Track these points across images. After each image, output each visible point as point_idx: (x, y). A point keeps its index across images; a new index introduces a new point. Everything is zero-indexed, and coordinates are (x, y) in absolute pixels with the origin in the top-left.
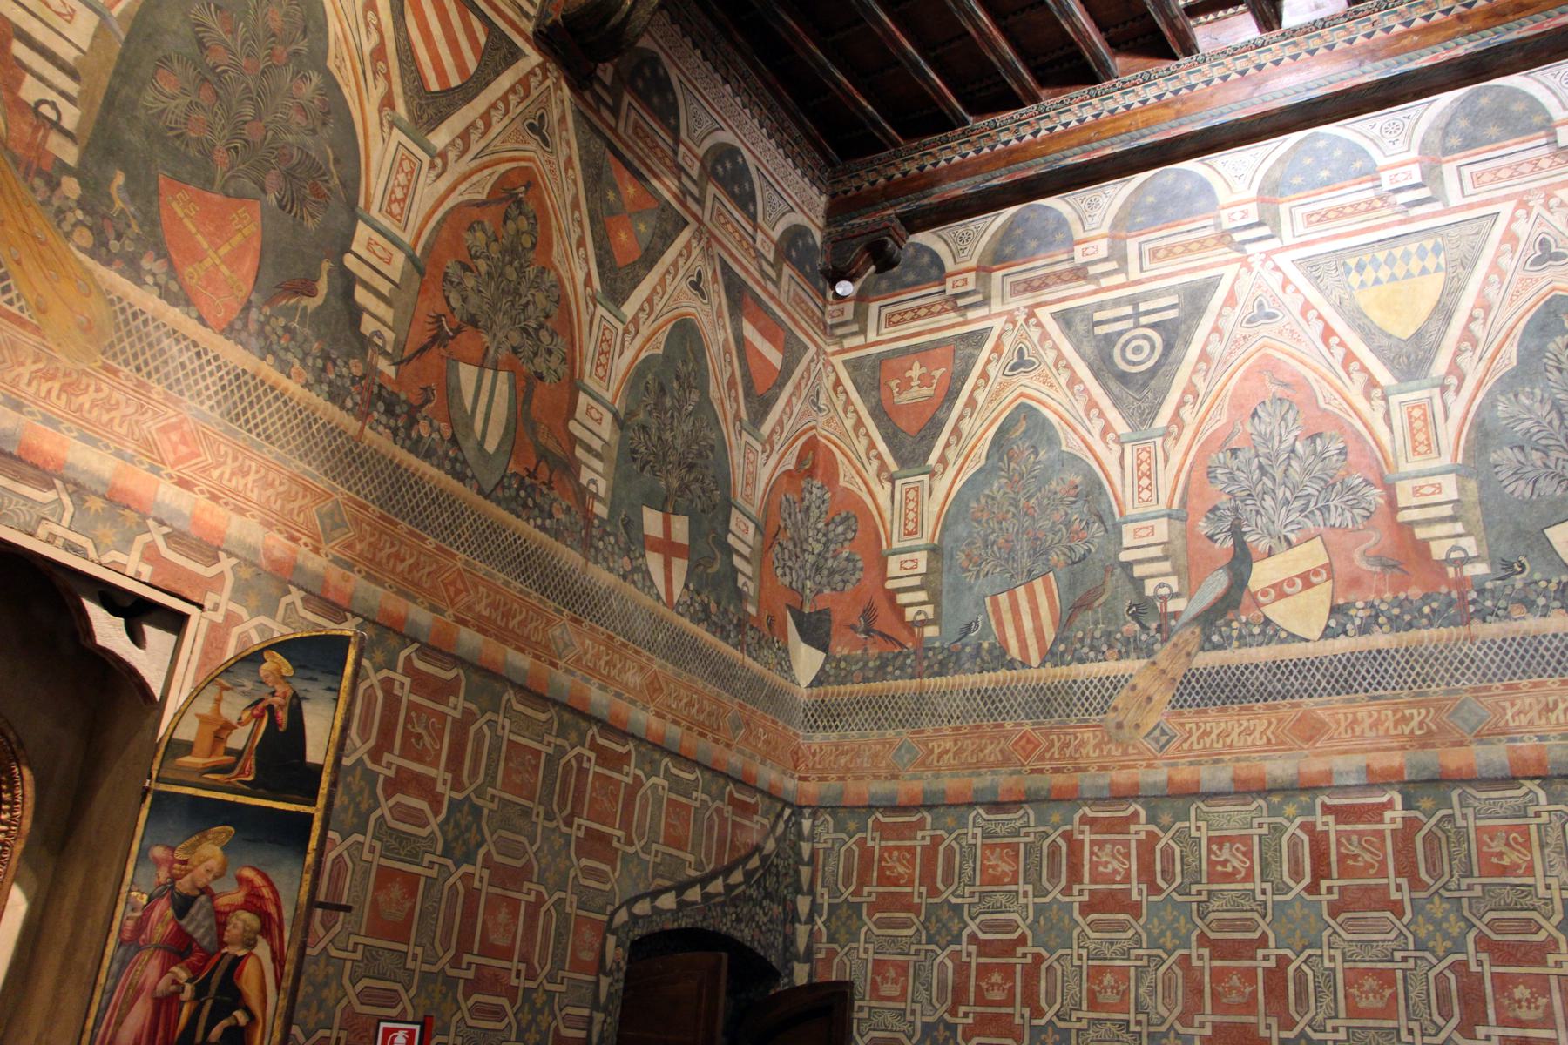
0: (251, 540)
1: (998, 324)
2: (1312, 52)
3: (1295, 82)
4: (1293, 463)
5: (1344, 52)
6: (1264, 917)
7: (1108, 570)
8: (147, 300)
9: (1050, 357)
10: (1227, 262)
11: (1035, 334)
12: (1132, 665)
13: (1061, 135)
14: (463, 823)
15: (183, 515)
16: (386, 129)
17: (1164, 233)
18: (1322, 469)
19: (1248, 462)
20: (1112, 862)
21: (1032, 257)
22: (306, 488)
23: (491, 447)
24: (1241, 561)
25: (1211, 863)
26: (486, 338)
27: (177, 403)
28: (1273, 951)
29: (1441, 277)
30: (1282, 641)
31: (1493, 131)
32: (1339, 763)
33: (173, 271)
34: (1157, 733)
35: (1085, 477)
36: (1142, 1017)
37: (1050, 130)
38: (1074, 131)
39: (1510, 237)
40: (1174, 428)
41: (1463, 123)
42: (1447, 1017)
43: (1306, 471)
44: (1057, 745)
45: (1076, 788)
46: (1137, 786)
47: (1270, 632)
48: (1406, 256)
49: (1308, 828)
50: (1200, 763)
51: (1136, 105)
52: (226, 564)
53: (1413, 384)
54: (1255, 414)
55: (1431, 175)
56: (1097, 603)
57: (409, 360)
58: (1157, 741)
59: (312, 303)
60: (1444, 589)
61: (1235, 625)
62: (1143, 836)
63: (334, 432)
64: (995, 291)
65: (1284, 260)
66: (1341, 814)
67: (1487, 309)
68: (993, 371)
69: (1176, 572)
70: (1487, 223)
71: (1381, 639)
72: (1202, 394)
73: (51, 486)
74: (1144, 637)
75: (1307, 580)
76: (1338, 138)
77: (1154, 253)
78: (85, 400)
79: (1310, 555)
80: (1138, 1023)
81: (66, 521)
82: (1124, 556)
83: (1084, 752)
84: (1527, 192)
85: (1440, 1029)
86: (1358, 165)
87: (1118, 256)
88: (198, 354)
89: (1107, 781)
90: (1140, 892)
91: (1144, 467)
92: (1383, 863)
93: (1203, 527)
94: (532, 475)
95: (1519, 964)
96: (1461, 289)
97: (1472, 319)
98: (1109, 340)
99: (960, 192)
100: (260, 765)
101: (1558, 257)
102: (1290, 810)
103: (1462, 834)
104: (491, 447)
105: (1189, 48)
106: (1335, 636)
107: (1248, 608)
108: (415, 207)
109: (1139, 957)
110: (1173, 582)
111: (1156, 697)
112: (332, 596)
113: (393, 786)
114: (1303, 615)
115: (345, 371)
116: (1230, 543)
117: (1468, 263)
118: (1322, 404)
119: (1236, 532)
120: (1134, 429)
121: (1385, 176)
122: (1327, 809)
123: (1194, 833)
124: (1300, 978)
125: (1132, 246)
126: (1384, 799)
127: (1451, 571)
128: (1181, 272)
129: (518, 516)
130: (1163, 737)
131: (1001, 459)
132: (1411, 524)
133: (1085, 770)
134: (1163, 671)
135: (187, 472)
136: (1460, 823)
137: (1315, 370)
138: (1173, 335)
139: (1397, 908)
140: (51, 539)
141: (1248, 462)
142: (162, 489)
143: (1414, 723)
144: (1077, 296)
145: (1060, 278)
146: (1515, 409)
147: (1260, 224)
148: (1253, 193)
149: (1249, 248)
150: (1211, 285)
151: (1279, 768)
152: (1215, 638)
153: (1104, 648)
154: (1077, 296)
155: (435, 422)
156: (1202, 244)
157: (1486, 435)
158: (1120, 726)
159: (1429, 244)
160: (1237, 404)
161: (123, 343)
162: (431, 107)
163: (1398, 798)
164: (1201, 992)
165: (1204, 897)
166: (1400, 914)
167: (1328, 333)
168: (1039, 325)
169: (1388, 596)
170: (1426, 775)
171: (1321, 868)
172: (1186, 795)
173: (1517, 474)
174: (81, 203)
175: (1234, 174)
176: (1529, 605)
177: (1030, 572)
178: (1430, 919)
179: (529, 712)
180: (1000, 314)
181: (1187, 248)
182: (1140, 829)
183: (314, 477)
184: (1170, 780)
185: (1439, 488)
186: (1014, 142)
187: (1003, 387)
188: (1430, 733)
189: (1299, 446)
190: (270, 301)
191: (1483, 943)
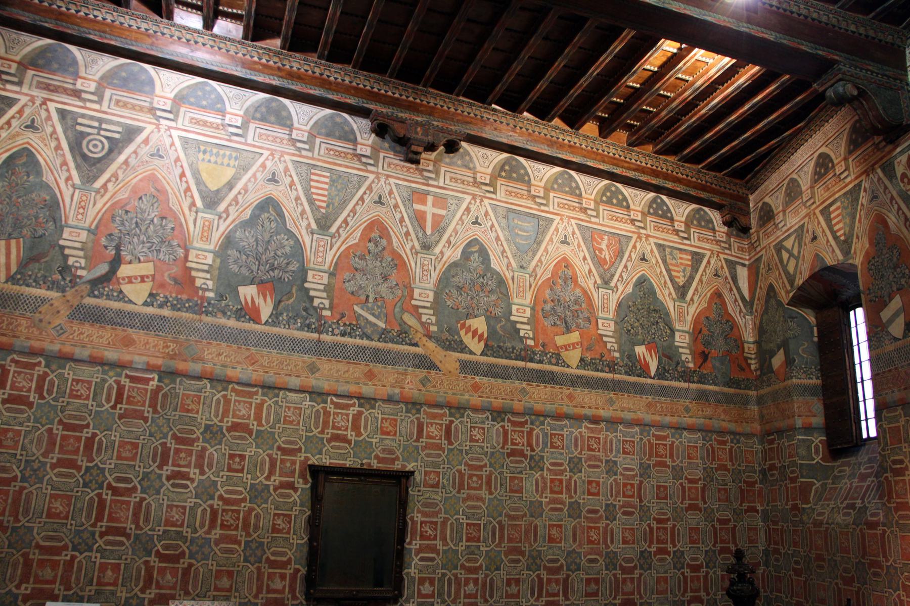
1: (24, 100)
2: (220, 49)
3: (203, 57)
4: (151, 226)
5: (232, 56)
6: (90, 416)
7: (53, 247)
9: (49, 130)
10: (150, 123)
11: (44, 114)
12: (54, 294)
13: (91, 20)
17: (125, 94)
18: (162, 234)
19: (132, 219)
20: (25, 383)
21: (53, 72)
24: (116, 262)
25: (71, 390)
28: (91, 430)
29: (234, 170)
30: (125, 302)
31: (273, 119)
32: (136, 358)
34: (58, 328)
35: (51, 197)
36: (24, 453)
37: (87, 14)
38: (98, 22)
39: (263, 166)
40: (102, 191)
41: (264, 109)
42: (154, 462)
43: (155, 231)
44: (6, 322)
45: (11, 345)
46: (43, 350)
47: (121, 296)
48: (224, 156)
49: (118, 382)
50: (75, 346)
51: (135, 27)
53: (209, 211)
54: (141, 198)
55: (244, 126)
56: (43, 260)
58: (58, 331)
60: (196, 299)
61: (107, 289)
62: (41, 373)
64: (27, 80)
65: (175, 133)
66: (133, 379)
67: (246, 191)
68: (14, 123)
69: (85, 257)
70: (257, 156)
71: (166, 312)
72: (120, 179)
74: (62, 283)
75: (143, 279)
76: (216, 90)
77: (118, 102)
79: (147, 269)
80: (22, 455)
82: (62, 242)
83: (20, 329)
84: (275, 150)
85: (151, 466)
86: (219, 106)
87: (99, 94)
89: (29, 344)
90: (34, 398)
91: (83, 204)
92: (145, 402)
93: (103, 241)
95: (184, 445)
96: (240, 179)
97: (239, 193)
98: (83, 135)
99: (23, 18)
101: (277, 182)
102: (111, 373)
103: (177, 395)
105: (170, 17)
106: (148, 306)
107: (114, 284)
109: (28, 426)
110: (83, 262)
111: (62, 312)
114: (137, 293)
116: (113, 252)
117: (245, 169)
118: (171, 205)
119: (118, 248)
120: (83, 183)
121: (228, 116)
122: (127, 376)
123: (66, 376)
124: (100, 443)
125: (108, 93)
126: (151, 376)
127: (200, 292)
128: (128, 118)
130: (61, 330)
131: (7, 172)
132: (191, 269)
133: (19, 337)
134: (68, 301)
136: (178, 391)
137: (172, 189)
138: (115, 146)
139: (146, 420)
141: (132, 219)
143: (170, 349)
144: (73, 105)
145: (65, 91)
146: (242, 236)
147: (170, 112)
148: (172, 96)
149: (162, 121)
150: (140, 130)
151: (111, 355)
152: (96, 293)
153: (41, 282)
154: (73, 105)
156: (141, 109)
157: (229, 242)
158: (41, 321)
159: (234, 155)
160: (134, 191)
163: (156, 377)
164: (55, 444)
165: (65, 404)
166: (146, 422)
167: (183, 175)
168: (47, 110)
169: (174, 295)
170: (169, 370)
171: (119, 399)
172: (65, 358)
173: (236, 262)
175: (169, 83)
176: (224, 313)
177: (10, 235)
178: (157, 426)
180: (27, 95)
181: (134, 107)
182: (40, 370)
184: (60, 351)
185: (206, 258)
186: (64, 9)
187: (18, 134)
188: (175, 354)
189: (155, 220)
191: (175, 436)
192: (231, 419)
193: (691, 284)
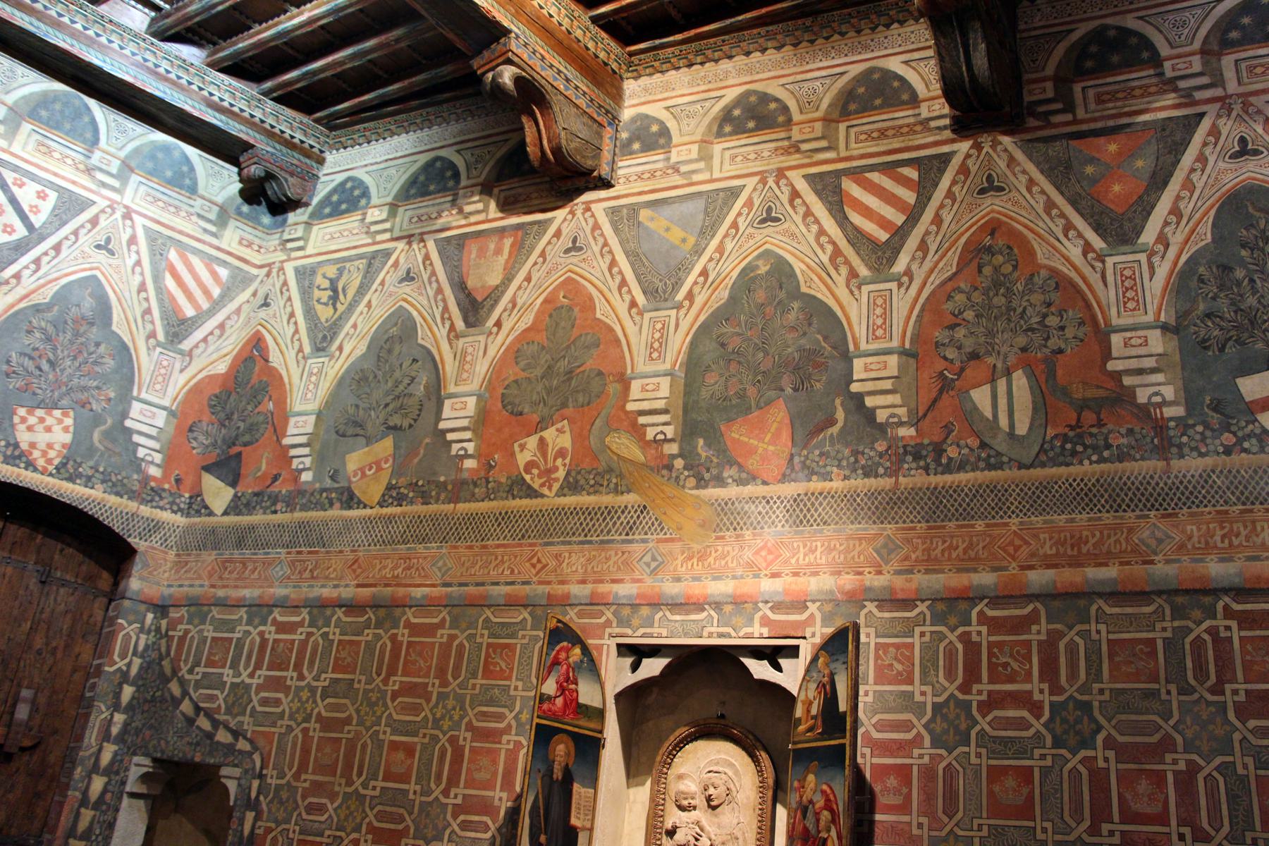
0: (827, 587)
8: (732, 491)
14: (1071, 719)
15: (779, 592)
16: (856, 292)
22: (860, 539)
23: (1022, 430)
26: (991, 360)
27: (760, 535)
33: (741, 467)
52: (813, 608)
57: (925, 415)
59: (835, 430)
63: (872, 495)
73: (703, 610)
78: (711, 560)
81: (715, 623)
88: (768, 502)
94: (1078, 424)
100: (823, 722)
104: (1022, 430)
108: (895, 321)
112: (900, 596)
113: (986, 707)
115: (872, 454)
129: (1068, 465)
135: (775, 568)
140: (710, 635)
142: (763, 584)
155: (962, 442)
161: (727, 519)
162: (881, 255)
174: (685, 468)
179: (1129, 610)
183: (865, 529)
190: (805, 447)
192: (986, 687)
193: (507, 287)
